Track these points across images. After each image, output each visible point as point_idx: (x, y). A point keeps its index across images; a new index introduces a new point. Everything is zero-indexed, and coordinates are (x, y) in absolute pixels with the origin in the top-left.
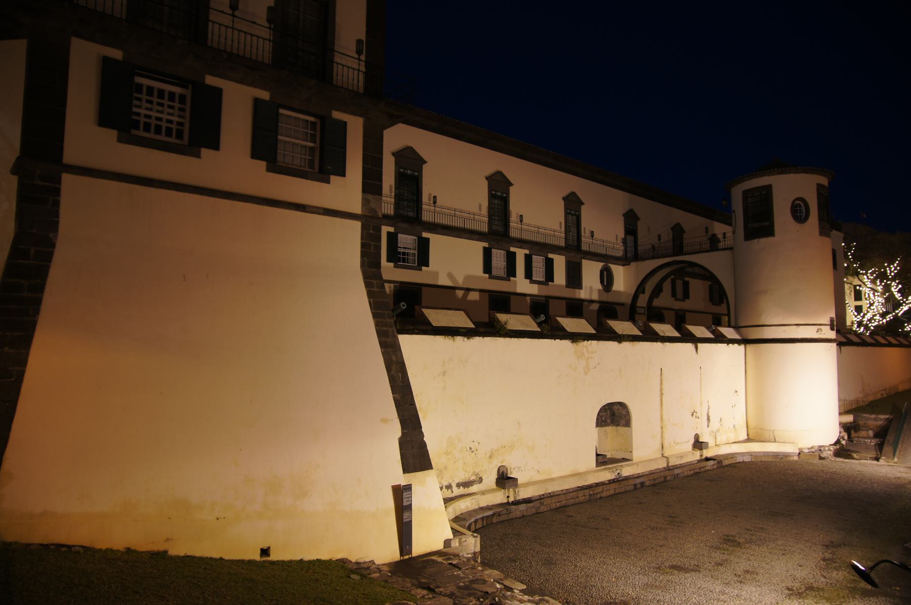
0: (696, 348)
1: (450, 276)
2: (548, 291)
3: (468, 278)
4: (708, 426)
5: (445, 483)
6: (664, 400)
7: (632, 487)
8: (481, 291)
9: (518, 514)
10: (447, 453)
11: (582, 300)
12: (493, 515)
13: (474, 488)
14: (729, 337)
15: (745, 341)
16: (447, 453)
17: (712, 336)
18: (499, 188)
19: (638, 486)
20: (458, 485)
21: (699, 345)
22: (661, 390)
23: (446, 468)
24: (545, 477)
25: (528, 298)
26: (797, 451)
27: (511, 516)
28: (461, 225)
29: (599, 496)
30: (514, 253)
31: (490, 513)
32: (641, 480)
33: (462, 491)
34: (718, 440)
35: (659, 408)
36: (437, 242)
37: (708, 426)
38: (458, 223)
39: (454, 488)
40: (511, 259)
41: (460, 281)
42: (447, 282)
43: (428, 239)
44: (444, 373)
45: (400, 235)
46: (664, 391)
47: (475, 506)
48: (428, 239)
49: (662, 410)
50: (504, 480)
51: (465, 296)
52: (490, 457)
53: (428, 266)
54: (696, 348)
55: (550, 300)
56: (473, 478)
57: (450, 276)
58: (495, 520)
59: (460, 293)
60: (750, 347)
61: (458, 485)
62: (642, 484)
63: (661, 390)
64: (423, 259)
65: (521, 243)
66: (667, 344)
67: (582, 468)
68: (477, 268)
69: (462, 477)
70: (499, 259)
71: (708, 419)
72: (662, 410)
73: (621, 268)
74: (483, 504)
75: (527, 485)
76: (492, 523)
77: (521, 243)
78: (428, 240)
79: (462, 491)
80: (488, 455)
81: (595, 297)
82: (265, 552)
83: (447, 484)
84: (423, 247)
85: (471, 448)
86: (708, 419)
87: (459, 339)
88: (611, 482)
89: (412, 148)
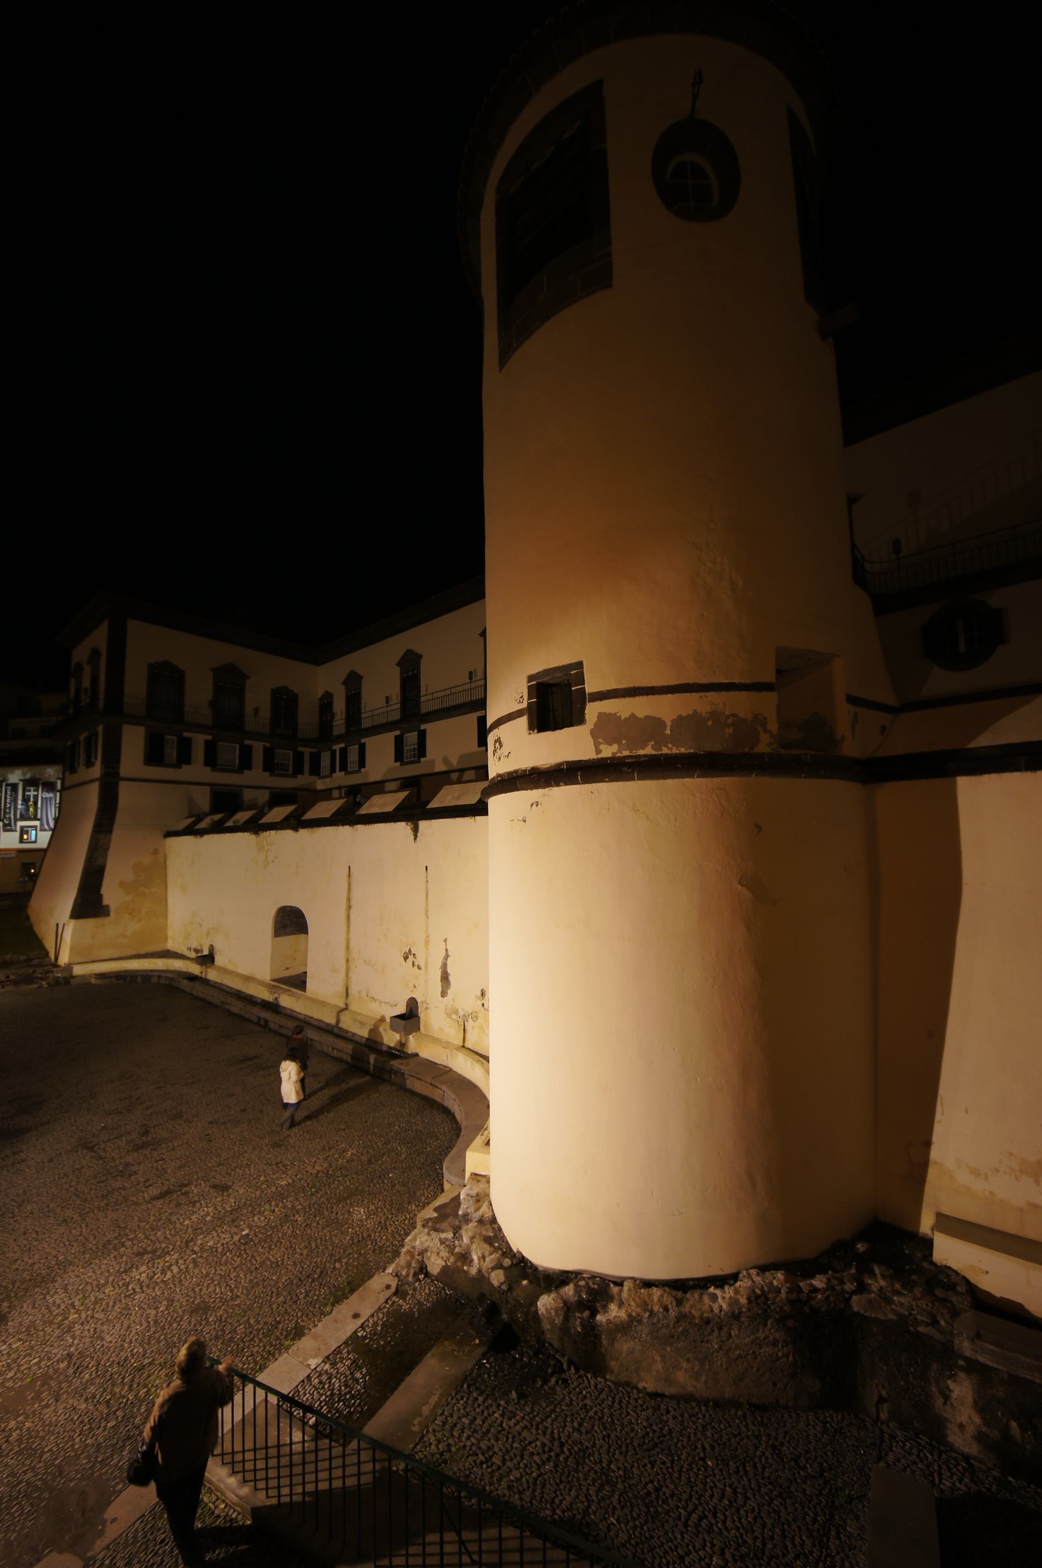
0: (416, 830)
1: (446, 761)
3: (462, 757)
4: (444, 994)
6: (351, 916)
21: (423, 824)
22: (349, 900)
28: (439, 707)
30: (189, 740)
34: (468, 1036)
35: (345, 927)
37: (444, 994)
38: (447, 704)
41: (455, 763)
46: (353, 903)
47: (184, 969)
49: (348, 932)
50: (208, 959)
54: (416, 830)
63: (349, 900)
66: (359, 826)
71: (445, 978)
72: (348, 932)
74: (171, 968)
75: (224, 971)
82: (208, 959)
86: (445, 978)
88: (266, 1005)
89: (182, 673)
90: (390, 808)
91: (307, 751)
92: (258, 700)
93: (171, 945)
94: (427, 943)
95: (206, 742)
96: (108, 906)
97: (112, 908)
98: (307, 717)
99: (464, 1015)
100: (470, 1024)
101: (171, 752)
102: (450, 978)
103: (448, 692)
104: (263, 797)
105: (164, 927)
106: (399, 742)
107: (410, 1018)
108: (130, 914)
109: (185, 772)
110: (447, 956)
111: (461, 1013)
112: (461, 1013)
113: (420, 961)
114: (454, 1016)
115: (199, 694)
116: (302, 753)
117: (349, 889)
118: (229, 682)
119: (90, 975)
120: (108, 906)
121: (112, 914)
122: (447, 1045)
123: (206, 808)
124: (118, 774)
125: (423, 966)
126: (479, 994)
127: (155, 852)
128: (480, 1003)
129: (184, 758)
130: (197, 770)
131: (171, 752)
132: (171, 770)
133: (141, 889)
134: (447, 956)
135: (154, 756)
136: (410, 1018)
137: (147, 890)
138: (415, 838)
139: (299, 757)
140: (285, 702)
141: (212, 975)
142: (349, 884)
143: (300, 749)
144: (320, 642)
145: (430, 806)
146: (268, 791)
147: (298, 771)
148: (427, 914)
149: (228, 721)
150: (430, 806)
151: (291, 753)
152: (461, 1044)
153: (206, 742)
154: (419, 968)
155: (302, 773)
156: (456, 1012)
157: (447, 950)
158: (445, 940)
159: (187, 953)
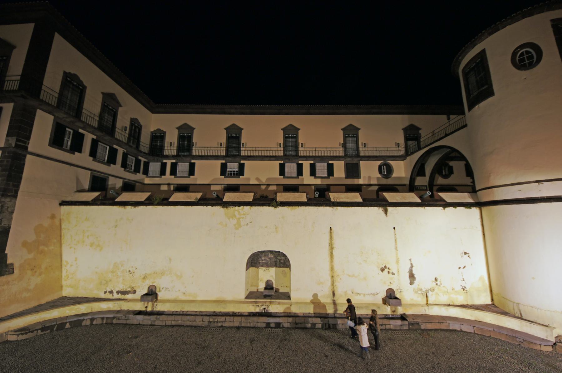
1: (257, 179)
2: (330, 181)
3: (268, 179)
4: (411, 283)
5: (109, 290)
6: (334, 253)
7: (264, 325)
8: (277, 185)
9: (135, 322)
10: (112, 272)
11: (361, 185)
12: (114, 318)
13: (129, 296)
14: (448, 200)
15: (479, 205)
16: (112, 272)
17: (419, 201)
18: (291, 134)
19: (272, 325)
20: (118, 292)
21: (390, 209)
23: (110, 280)
24: (191, 298)
25: (313, 187)
26: (554, 340)
27: (128, 322)
29: (220, 324)
31: (112, 316)
32: (277, 320)
33: (120, 296)
34: (429, 299)
35: (328, 259)
36: (247, 164)
39: (115, 294)
40: (164, 166)
41: (264, 181)
42: (256, 182)
43: (333, 164)
44: (116, 226)
45: (286, 164)
48: (333, 164)
50: (152, 294)
51: (266, 189)
52: (144, 278)
53: (243, 175)
55: (331, 187)
56: (129, 289)
57: (257, 179)
58: (114, 321)
59: (263, 187)
60: (485, 209)
61: (118, 292)
62: (278, 325)
64: (241, 171)
65: (306, 158)
67: (229, 297)
68: (276, 173)
69: (121, 287)
70: (291, 168)
71: (412, 276)
73: (402, 162)
75: (164, 301)
76: (112, 324)
77: (306, 158)
78: (302, 164)
79: (120, 296)
80: (143, 277)
81: (374, 182)
83: (110, 290)
84: (242, 166)
85: (129, 271)
86: (412, 276)
87: (129, 208)
88: (140, 313)
89: (85, 88)
90: (90, 199)
91: (143, 160)
92: (123, 121)
93: (67, 292)
94: (398, 262)
95: (93, 139)
96: (12, 264)
97: (16, 266)
98: (145, 140)
99: (426, 290)
100: (429, 294)
101: (68, 141)
102: (415, 276)
103: (314, 149)
104: (119, 184)
105: (60, 279)
106: (223, 166)
107: (391, 297)
108: (32, 270)
109: (75, 158)
110: (412, 266)
111: (424, 290)
112: (424, 290)
113: (393, 270)
114: (420, 292)
115: (92, 106)
116: (140, 161)
117: (331, 238)
118: (110, 105)
119: (7, 333)
120: (12, 264)
121: (16, 271)
122: (422, 306)
123: (87, 186)
124: (26, 148)
125: (396, 273)
126: (434, 280)
127: (53, 217)
128: (435, 284)
129: (77, 147)
130: (83, 158)
131: (68, 141)
132: (67, 154)
133: (41, 247)
134: (412, 266)
135: (57, 141)
136: (391, 297)
137: (46, 249)
138: (386, 213)
139: (138, 162)
140: (135, 128)
141: (160, 307)
142: (331, 237)
143: (140, 158)
144: (160, 99)
145: (116, 200)
146: (122, 180)
147: (137, 170)
148: (396, 248)
149: (106, 127)
150: (116, 200)
151: (134, 159)
152: (426, 303)
153: (93, 139)
154: (393, 274)
155: (139, 172)
156: (421, 290)
157: (411, 264)
158: (410, 260)
159: (103, 296)
